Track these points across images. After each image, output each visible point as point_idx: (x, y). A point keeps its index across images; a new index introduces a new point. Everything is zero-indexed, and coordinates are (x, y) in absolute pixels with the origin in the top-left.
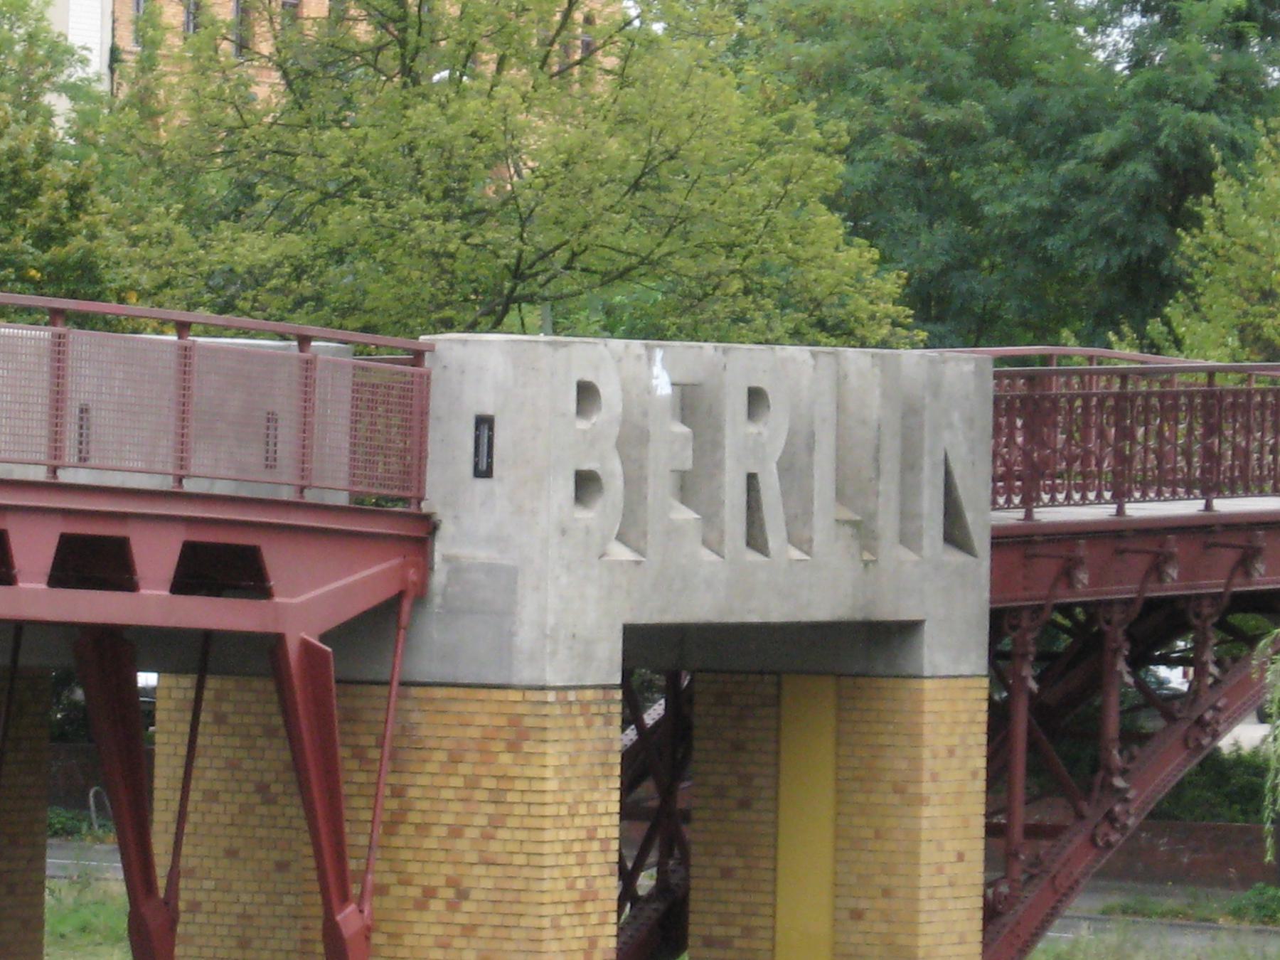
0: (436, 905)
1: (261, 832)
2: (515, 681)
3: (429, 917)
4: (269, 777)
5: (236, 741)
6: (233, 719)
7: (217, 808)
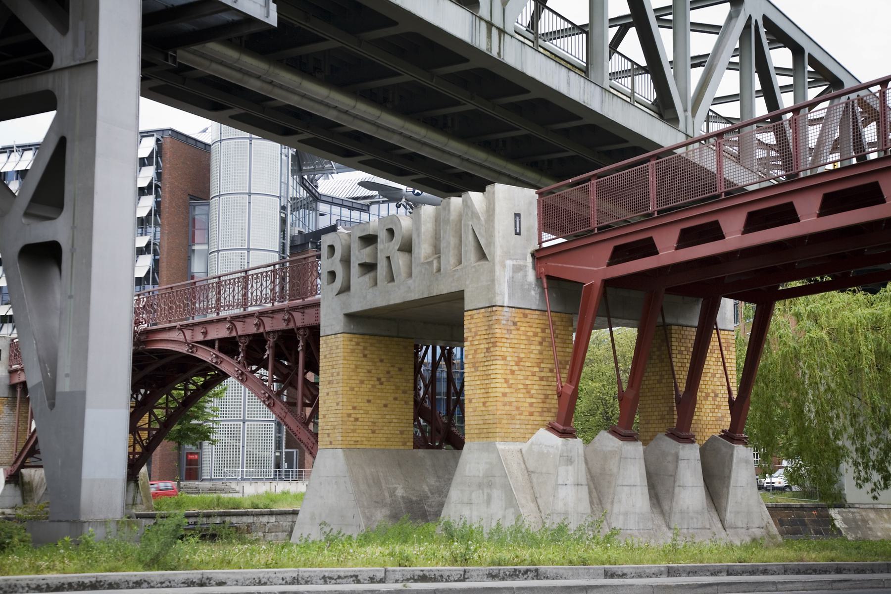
0: (710, 398)
1: (379, 394)
2: (726, 328)
3: (708, 402)
4: (381, 376)
5: (370, 364)
6: (368, 356)
7: (364, 386)
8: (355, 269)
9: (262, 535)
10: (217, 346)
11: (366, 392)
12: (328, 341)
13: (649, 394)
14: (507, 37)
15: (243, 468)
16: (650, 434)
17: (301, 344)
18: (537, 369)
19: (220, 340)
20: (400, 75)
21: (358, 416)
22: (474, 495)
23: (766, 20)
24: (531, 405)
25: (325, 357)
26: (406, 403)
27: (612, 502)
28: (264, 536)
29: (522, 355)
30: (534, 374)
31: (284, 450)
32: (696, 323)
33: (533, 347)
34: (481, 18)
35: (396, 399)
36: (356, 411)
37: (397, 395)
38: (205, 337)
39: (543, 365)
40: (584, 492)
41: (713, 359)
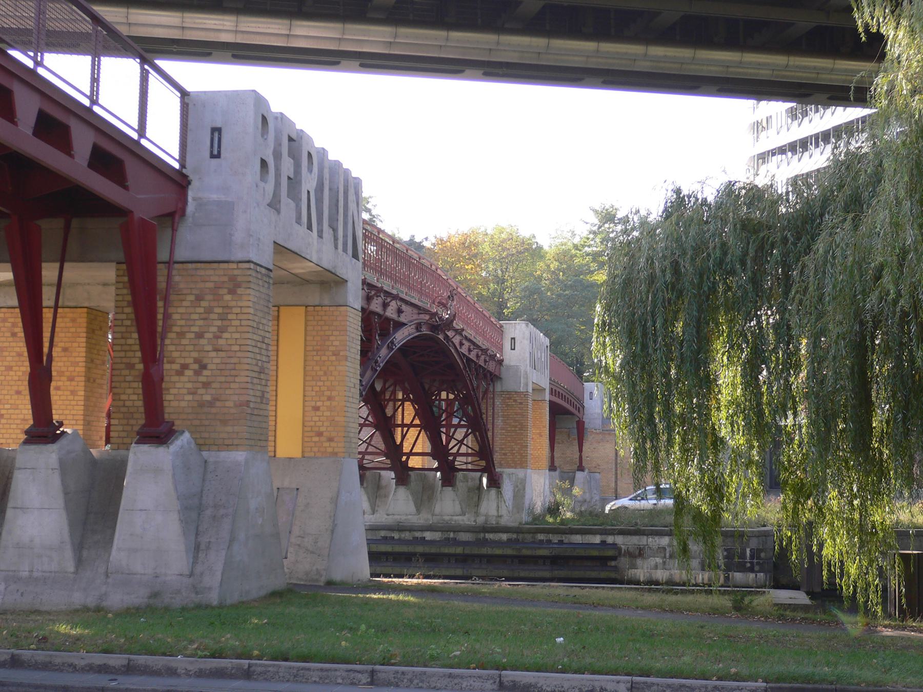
0: (188, 373)
2: (233, 259)
7: (11, 373)
9: (661, 561)
11: (15, 381)
28: (664, 563)
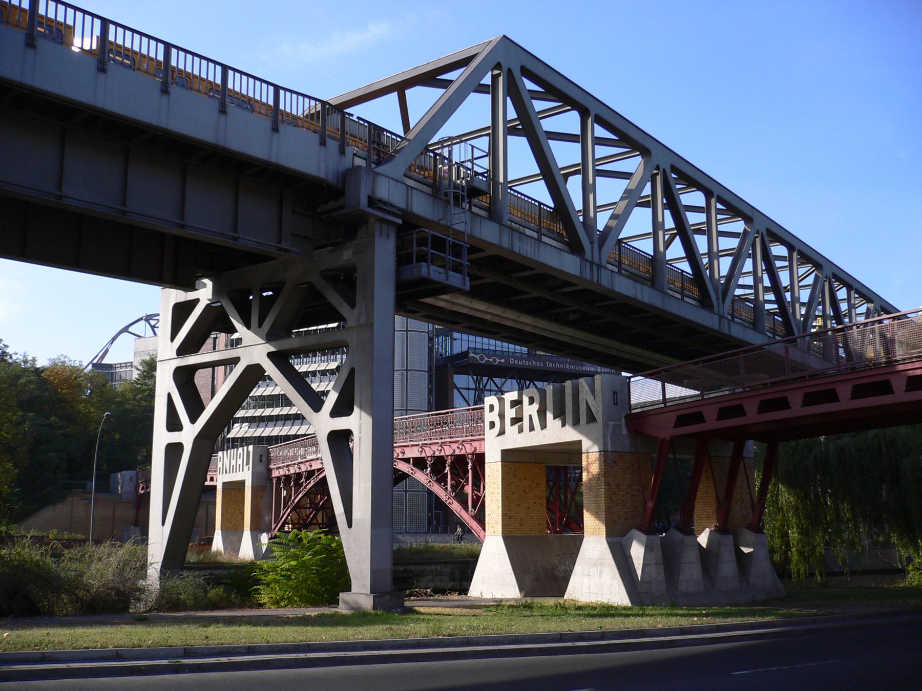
8: (508, 422)
10: (411, 462)
12: (490, 466)
13: (700, 501)
14: (603, 270)
15: (406, 525)
16: (701, 526)
17: (470, 465)
18: (629, 490)
19: (414, 458)
20: (531, 293)
21: (512, 515)
22: (591, 570)
23: (768, 231)
24: (626, 513)
25: (489, 476)
26: (542, 505)
27: (679, 574)
28: (433, 578)
29: (620, 482)
30: (627, 493)
31: (434, 512)
32: (730, 454)
33: (626, 476)
34: (586, 260)
35: (535, 503)
36: (510, 512)
37: (536, 501)
38: (403, 456)
39: (633, 487)
40: (661, 568)
41: (741, 477)
